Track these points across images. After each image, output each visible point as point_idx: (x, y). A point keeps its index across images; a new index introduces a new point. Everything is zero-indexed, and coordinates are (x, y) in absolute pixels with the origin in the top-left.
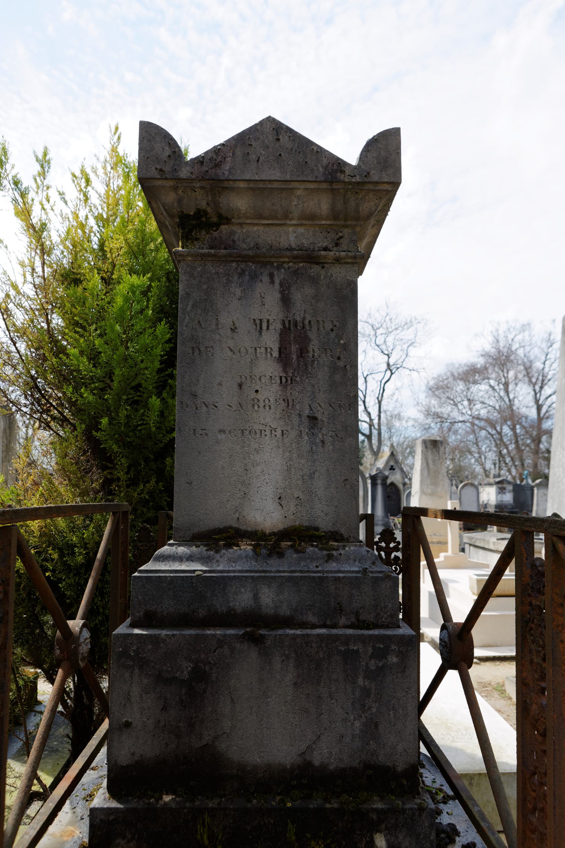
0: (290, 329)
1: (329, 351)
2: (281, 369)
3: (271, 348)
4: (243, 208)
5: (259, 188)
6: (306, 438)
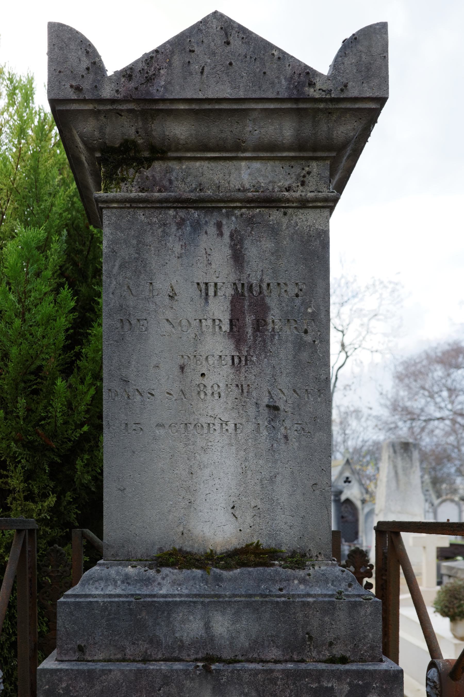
0: (243, 295)
1: (292, 321)
2: (232, 347)
3: (220, 320)
4: (182, 137)
5: (204, 110)
6: (265, 433)
